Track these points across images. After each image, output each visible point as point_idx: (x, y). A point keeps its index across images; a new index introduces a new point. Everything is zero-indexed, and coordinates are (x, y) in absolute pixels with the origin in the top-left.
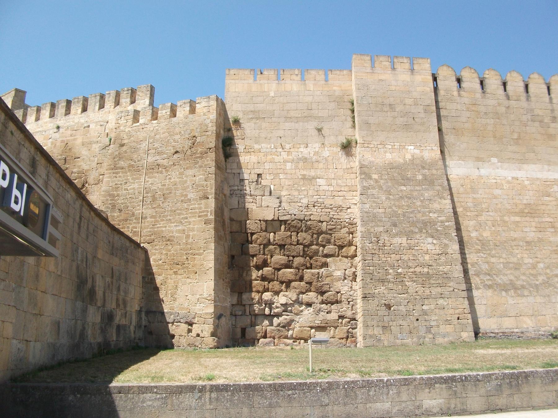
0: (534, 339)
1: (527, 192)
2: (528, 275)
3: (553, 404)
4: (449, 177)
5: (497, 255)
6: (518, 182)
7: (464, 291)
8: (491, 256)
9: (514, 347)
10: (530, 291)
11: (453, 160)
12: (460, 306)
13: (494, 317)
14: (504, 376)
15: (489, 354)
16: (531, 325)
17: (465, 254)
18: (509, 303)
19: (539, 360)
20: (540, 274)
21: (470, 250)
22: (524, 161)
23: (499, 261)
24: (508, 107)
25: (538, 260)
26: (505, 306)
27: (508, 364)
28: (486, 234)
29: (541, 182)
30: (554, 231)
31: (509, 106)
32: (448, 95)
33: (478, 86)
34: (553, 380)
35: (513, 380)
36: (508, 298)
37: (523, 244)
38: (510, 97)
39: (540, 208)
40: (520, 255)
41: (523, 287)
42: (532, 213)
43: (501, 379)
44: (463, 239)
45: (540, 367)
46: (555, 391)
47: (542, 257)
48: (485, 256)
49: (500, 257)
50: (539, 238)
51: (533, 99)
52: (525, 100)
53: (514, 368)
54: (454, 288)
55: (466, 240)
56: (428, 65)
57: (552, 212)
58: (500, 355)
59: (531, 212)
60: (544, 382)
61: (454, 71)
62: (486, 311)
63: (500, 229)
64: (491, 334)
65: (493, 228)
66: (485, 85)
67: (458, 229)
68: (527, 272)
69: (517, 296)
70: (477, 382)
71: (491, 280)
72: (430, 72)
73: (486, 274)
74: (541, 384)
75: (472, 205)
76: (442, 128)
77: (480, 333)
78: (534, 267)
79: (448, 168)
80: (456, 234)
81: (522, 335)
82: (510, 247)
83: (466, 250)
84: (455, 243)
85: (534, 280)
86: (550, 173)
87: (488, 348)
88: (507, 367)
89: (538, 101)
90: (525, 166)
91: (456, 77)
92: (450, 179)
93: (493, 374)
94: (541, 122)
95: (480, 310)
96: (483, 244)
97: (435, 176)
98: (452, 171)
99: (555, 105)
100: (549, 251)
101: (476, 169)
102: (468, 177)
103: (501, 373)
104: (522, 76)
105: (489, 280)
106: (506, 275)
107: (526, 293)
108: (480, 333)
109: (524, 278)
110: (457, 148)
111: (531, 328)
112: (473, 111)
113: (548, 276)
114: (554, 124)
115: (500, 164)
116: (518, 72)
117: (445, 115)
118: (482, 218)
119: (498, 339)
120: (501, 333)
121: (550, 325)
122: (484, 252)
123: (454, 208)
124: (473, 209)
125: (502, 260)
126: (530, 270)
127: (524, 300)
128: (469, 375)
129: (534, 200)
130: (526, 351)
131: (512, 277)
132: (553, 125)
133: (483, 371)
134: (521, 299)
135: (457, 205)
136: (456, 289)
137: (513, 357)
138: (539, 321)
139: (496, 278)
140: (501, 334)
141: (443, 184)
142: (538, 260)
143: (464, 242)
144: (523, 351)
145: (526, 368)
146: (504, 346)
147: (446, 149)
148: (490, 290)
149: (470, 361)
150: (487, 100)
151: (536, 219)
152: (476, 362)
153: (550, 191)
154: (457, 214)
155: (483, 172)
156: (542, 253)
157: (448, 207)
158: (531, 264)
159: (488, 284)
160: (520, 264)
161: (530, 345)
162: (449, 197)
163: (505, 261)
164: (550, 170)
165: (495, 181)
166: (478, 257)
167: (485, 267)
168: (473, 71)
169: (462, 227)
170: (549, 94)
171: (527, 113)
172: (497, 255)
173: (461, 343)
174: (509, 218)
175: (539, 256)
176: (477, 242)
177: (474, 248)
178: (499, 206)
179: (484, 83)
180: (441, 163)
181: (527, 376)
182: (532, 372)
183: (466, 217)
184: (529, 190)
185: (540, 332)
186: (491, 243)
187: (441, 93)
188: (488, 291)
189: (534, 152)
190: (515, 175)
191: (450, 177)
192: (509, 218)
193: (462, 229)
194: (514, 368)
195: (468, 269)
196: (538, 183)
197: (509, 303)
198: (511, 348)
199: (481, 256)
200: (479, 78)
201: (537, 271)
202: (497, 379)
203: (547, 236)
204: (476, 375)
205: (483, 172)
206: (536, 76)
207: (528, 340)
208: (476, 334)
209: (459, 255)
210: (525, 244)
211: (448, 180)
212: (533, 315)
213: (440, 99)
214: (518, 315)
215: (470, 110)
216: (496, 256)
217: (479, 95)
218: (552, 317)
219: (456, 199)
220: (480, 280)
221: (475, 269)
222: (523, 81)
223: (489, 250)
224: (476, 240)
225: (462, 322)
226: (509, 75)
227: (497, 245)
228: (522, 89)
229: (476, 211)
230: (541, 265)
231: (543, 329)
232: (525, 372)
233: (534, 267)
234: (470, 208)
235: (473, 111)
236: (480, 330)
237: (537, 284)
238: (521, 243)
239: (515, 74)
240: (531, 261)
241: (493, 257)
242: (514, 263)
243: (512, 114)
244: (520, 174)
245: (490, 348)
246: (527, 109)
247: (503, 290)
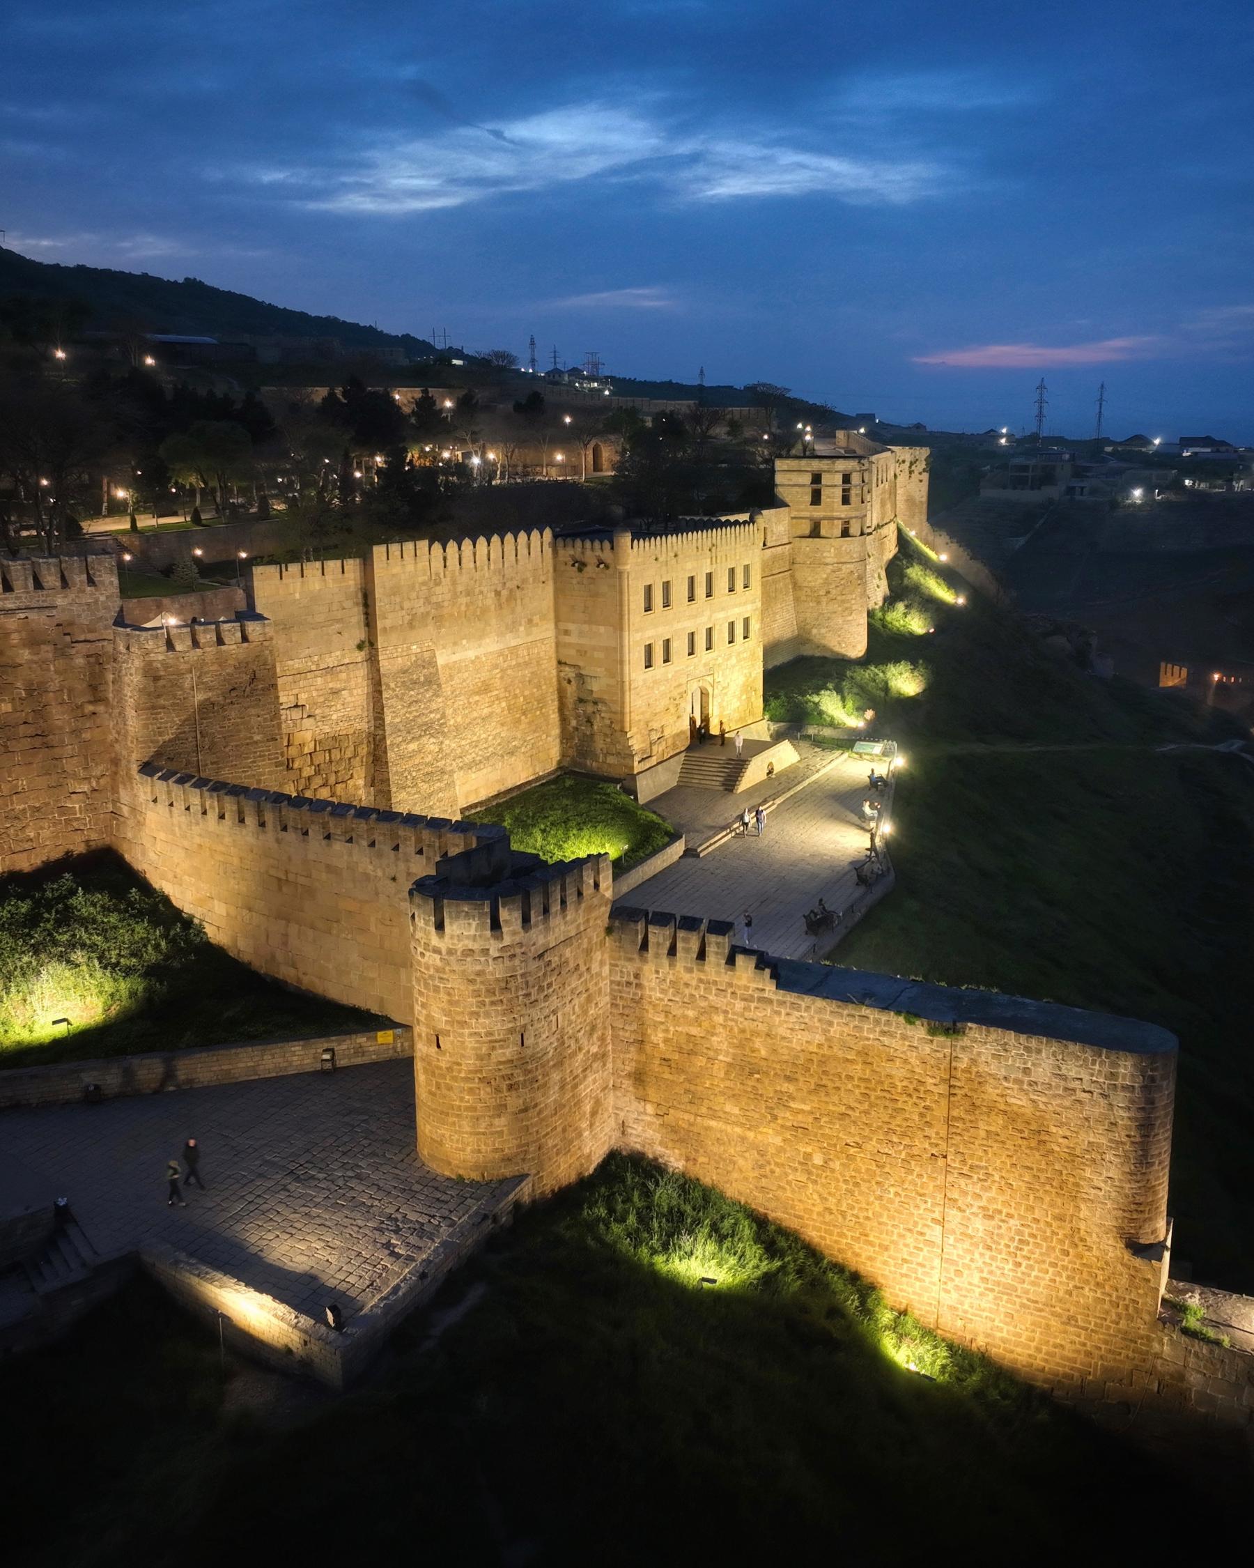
78: (486, 739)
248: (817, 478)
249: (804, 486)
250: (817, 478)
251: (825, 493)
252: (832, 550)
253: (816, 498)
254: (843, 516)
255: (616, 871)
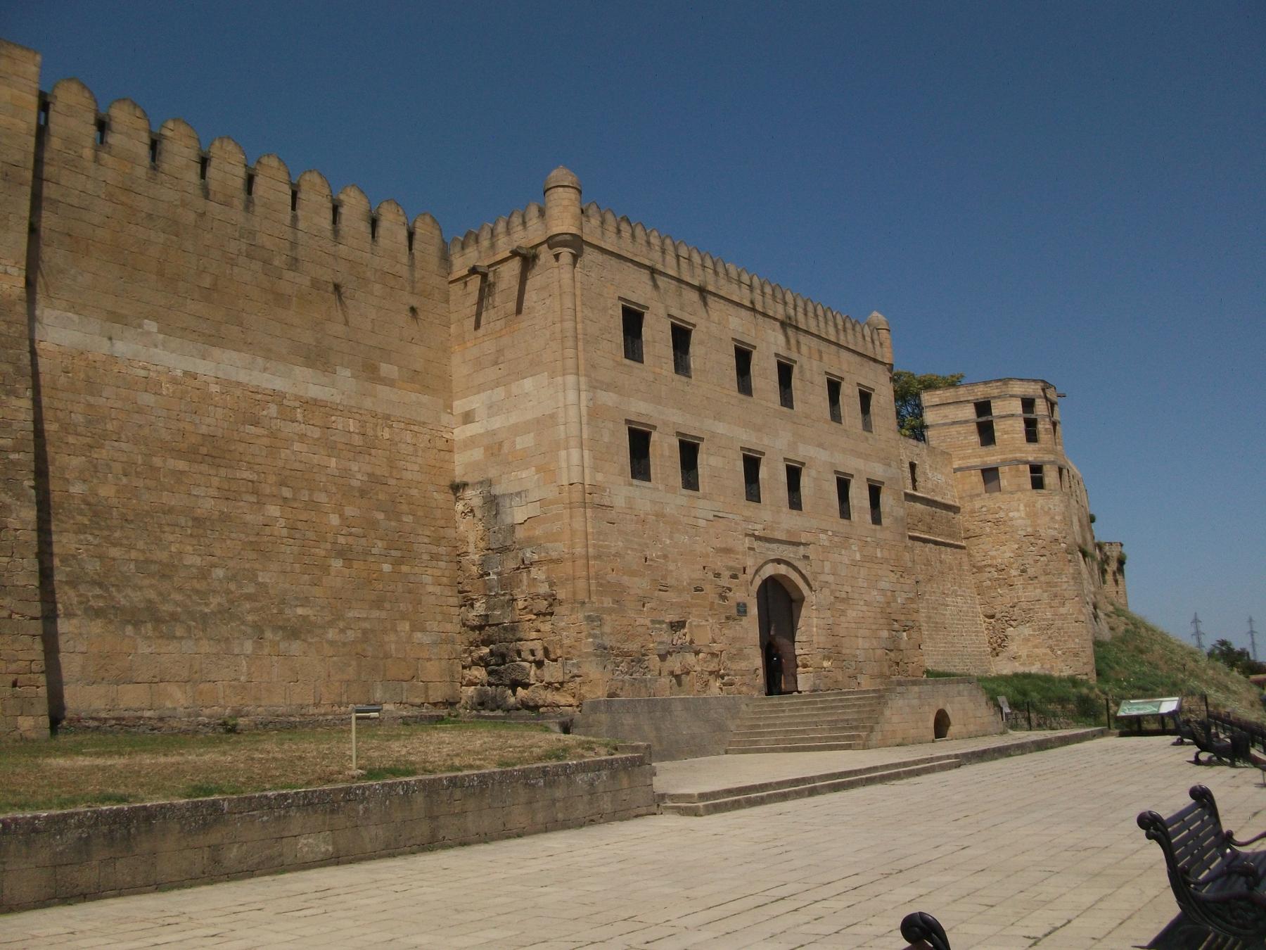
0: (186, 732)
1: (211, 408)
2: (188, 592)
3: (202, 876)
4: (36, 346)
5: (125, 542)
6: (196, 383)
7: (36, 619)
8: (112, 543)
9: (136, 752)
10: (189, 627)
11: (54, 308)
12: (21, 655)
13: (100, 683)
14: (98, 817)
15: (73, 769)
16: (182, 701)
17: (49, 532)
18: (140, 651)
19: (184, 780)
20: (214, 591)
21: (64, 525)
22: (215, 340)
23: (127, 557)
24: (203, 215)
25: (215, 560)
26: (130, 658)
27: (111, 790)
28: (106, 492)
29: (245, 392)
30: (255, 501)
31: (205, 213)
32: (70, 152)
33: (143, 151)
34: (205, 824)
35: (117, 826)
36: (139, 640)
37: (186, 521)
38: (211, 193)
39: (233, 448)
40: (178, 545)
41: (174, 617)
42: (215, 457)
43: (90, 827)
44: (49, 497)
45: (181, 796)
46: (209, 847)
47: (223, 555)
48: (96, 542)
49: (131, 547)
50: (223, 513)
51: (259, 210)
52: (241, 208)
53: (122, 799)
54: (12, 612)
55: (56, 499)
56: (34, 69)
57: (259, 460)
58: (99, 770)
59: (214, 454)
60: (187, 828)
61: (95, 101)
62: (83, 667)
63: (140, 483)
64: (91, 721)
65: (125, 480)
66: (160, 153)
67: (41, 472)
68: (187, 586)
69: (158, 638)
70: (33, 835)
71: (105, 598)
72: (36, 86)
73: (94, 583)
74: (179, 833)
75: (82, 420)
76: (40, 226)
77: (64, 718)
78: (204, 574)
79: (37, 325)
80: (32, 483)
81: (160, 724)
82: (156, 525)
83: (53, 524)
84: (27, 504)
85: (200, 604)
86: (266, 375)
87: (79, 753)
88: (108, 798)
89: (268, 216)
90: (217, 352)
91: (96, 115)
92: (38, 351)
93: (72, 813)
94: (267, 262)
95: (70, 665)
96: (96, 514)
97: (3, 338)
98: (47, 334)
99: (300, 234)
100: (240, 543)
101: (105, 340)
102: (82, 353)
103: (91, 812)
104: (244, 154)
105: (98, 597)
106: (141, 588)
107: (179, 632)
108: (64, 718)
109: (178, 597)
110: (68, 282)
111: (182, 709)
112: (122, 204)
113: (231, 596)
114: (292, 274)
115: (161, 336)
116: (236, 144)
117: (53, 197)
118: (102, 454)
119: (105, 733)
120: (114, 719)
121: (223, 703)
122: (96, 532)
123: (38, 421)
124: (82, 428)
125: (133, 554)
126: (196, 580)
127: (173, 646)
128: (15, 820)
129: (223, 429)
130: (162, 760)
131: (152, 595)
132: (289, 275)
133: (51, 808)
134: (168, 645)
135: (48, 414)
136: (17, 614)
137: (128, 774)
138: (201, 693)
139: (115, 594)
140: (114, 722)
141: (19, 360)
142: (215, 560)
143: (52, 503)
144: (153, 761)
145: (151, 799)
146: (114, 749)
147: (40, 279)
148: (99, 621)
149: (23, 784)
150: (159, 186)
151: (223, 472)
152: (39, 786)
153: (261, 414)
154: (43, 437)
155: (120, 347)
156: (224, 546)
157: (23, 416)
158: (198, 569)
159: (96, 607)
160: (173, 566)
161: (173, 745)
162: (29, 393)
163: (142, 558)
164: (267, 368)
165: (143, 373)
166: (80, 542)
167: (92, 567)
168: (138, 113)
169: (51, 468)
170: (294, 208)
171: (241, 236)
172: (125, 542)
173: (17, 741)
174: (164, 461)
175: (218, 552)
176: (83, 506)
177: (72, 522)
178: (146, 431)
179: (159, 147)
180: (21, 309)
181: (149, 815)
182: (162, 807)
183: (63, 446)
184: (216, 406)
185: (200, 718)
186: (114, 514)
187: (55, 143)
188: (93, 623)
189: (241, 324)
190: (191, 368)
191: (40, 347)
192: (164, 461)
193: (51, 474)
194: (122, 799)
195: (52, 569)
196: (238, 392)
197: (140, 651)
198: (130, 754)
199: (88, 541)
200: (151, 132)
201: (208, 584)
202: (80, 825)
203: (240, 511)
204: (31, 818)
205: (120, 347)
206: (274, 162)
207: (172, 735)
208: (56, 718)
209: (35, 534)
210: (190, 524)
211: (33, 353)
212: (188, 681)
213: (47, 155)
214: (156, 680)
215: (115, 201)
216: (121, 545)
217: (141, 171)
218: (230, 686)
219: (45, 401)
220: (77, 596)
221: (70, 569)
222: (246, 166)
223: (109, 528)
224: (80, 502)
225: (22, 692)
226: (217, 143)
227: (129, 518)
228: (239, 183)
229: (89, 434)
230: (219, 573)
231: (207, 711)
232: (145, 808)
233: (204, 574)
234: (76, 426)
235: (122, 204)
236: (66, 713)
237: (206, 614)
238: (182, 521)
239: (230, 146)
240: (197, 561)
241: (114, 545)
242: (160, 563)
243: (208, 232)
244: (204, 368)
245: (83, 754)
246: (241, 228)
247: (129, 622)
248: (983, 408)
249: (966, 422)
250: (983, 408)
251: (998, 427)
252: (1022, 507)
253: (986, 434)
254: (1030, 459)
255: (1049, 746)
